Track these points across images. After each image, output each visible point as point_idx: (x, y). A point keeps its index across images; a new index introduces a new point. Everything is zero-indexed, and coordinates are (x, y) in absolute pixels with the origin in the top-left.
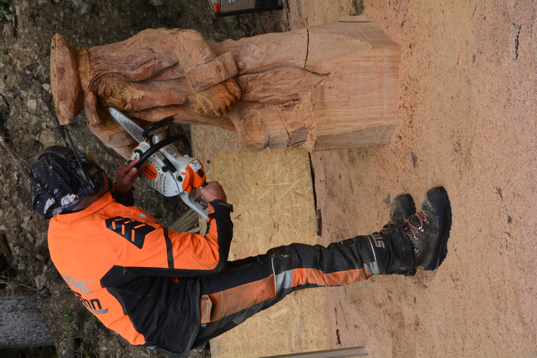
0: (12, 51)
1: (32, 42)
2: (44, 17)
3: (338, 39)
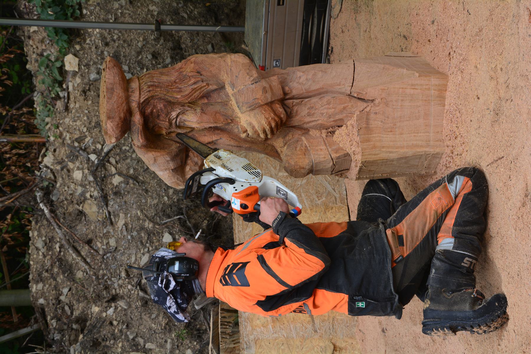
0: (62, 125)
1: (82, 115)
2: (94, 92)
3: (384, 68)
